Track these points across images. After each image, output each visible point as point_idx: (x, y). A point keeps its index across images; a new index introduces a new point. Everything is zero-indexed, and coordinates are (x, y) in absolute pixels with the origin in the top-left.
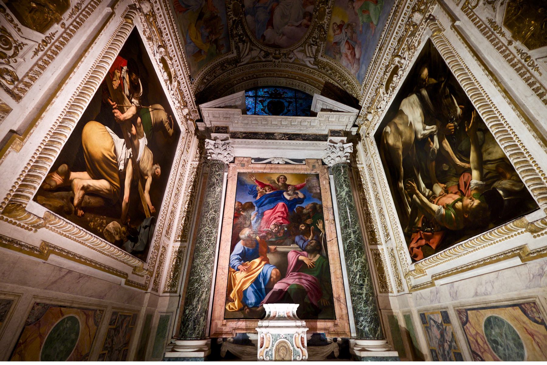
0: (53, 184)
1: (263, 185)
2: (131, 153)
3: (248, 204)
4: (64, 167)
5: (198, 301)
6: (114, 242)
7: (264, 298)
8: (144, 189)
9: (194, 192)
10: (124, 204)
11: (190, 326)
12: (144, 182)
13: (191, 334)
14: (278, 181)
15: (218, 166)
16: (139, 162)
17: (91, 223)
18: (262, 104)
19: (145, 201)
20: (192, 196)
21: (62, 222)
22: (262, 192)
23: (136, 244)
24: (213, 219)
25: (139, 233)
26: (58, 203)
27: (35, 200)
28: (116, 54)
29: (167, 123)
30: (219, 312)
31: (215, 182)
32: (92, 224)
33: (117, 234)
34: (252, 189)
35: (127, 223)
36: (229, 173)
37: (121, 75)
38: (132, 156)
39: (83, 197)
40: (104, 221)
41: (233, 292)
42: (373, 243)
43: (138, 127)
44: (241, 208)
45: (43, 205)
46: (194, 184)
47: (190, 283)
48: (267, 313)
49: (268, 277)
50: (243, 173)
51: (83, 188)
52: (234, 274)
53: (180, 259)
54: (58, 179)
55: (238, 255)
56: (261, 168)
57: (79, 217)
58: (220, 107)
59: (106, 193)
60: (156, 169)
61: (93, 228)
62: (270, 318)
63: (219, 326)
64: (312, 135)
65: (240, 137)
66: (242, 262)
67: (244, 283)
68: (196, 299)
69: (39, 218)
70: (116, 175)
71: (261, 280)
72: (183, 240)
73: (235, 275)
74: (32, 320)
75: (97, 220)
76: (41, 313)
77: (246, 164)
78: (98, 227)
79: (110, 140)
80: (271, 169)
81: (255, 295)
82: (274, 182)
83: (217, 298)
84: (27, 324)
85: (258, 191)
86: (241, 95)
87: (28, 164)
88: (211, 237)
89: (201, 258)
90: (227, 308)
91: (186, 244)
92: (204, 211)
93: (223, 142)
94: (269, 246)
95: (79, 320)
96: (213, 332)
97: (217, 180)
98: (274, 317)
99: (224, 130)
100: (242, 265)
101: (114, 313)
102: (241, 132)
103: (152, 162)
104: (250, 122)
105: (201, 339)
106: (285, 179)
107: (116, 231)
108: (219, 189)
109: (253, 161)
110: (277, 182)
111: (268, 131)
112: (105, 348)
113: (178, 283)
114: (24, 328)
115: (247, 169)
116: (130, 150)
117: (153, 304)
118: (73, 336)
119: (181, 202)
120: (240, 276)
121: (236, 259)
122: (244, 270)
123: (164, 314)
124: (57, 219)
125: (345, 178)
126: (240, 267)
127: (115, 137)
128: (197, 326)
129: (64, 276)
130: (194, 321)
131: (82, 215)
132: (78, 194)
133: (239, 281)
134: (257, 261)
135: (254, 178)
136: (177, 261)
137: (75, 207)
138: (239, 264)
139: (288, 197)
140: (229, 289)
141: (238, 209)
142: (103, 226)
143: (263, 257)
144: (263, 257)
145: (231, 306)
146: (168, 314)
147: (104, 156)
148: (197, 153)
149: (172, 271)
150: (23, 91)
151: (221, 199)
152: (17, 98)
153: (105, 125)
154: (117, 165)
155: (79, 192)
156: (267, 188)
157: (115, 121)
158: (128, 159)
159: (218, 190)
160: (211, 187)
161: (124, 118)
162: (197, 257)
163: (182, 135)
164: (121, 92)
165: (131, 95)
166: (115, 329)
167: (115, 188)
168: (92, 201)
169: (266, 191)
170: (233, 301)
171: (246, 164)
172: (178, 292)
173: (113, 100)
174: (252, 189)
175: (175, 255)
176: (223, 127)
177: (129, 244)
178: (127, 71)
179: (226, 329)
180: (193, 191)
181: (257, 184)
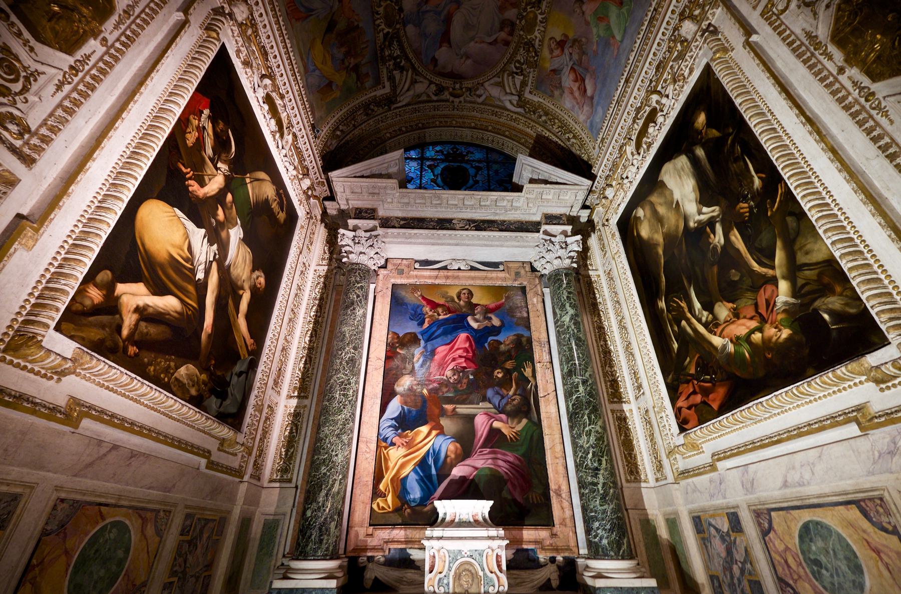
0: (88, 303)
1: (434, 305)
2: (217, 252)
3: (409, 336)
4: (105, 275)
5: (327, 495)
7: (435, 490)
8: (238, 312)
9: (319, 317)
10: (204, 336)
11: (313, 537)
12: (238, 299)
13: (315, 551)
14: (459, 297)
16: (229, 266)
17: (149, 367)
18: (432, 171)
19: (239, 330)
21: (102, 366)
22: (433, 316)
24: (352, 360)
25: (228, 384)
26: (96, 334)
27: (58, 328)
28: (192, 88)
29: (276, 202)
30: (362, 513)
32: (152, 368)
33: (193, 386)
37: (199, 124)
38: (217, 256)
39: (137, 325)
40: (172, 364)
42: (615, 400)
44: (397, 343)
45: (71, 337)
47: (313, 465)
48: (441, 516)
49: (443, 455)
51: (137, 310)
52: (385, 452)
53: (296, 426)
54: (95, 294)
55: (392, 419)
56: (430, 277)
57: (130, 357)
59: (174, 317)
60: (257, 278)
62: (445, 524)
63: (361, 537)
64: (515, 222)
65: (397, 225)
66: (400, 431)
67: (403, 466)
68: (323, 493)
69: (64, 359)
70: (191, 288)
71: (431, 461)
72: (302, 394)
73: (387, 453)
75: (161, 362)
76: (67, 516)
78: (162, 373)
79: (182, 231)
80: (447, 277)
82: (453, 300)
83: (357, 491)
85: (425, 315)
88: (348, 390)
90: (375, 507)
91: (306, 402)
94: (444, 406)
97: (358, 296)
98: (453, 521)
100: (400, 436)
101: (188, 516)
104: (412, 201)
105: (331, 559)
106: (471, 294)
107: (191, 380)
108: (361, 312)
109: (417, 266)
110: (456, 300)
111: (442, 216)
112: (173, 573)
115: (408, 278)
116: (215, 247)
117: (253, 500)
118: (120, 553)
119: (298, 333)
120: (395, 455)
121: (390, 426)
122: (403, 444)
125: (569, 293)
126: (396, 440)
131: (136, 355)
132: (129, 320)
134: (424, 429)
135: (419, 293)
136: (291, 429)
137: (124, 341)
138: (394, 435)
139: (475, 325)
140: (378, 476)
141: (393, 344)
142: (169, 373)
143: (434, 424)
144: (434, 424)
145: (381, 504)
146: (277, 517)
149: (283, 446)
150: (39, 150)
152: (29, 161)
153: (173, 205)
154: (193, 272)
155: (130, 315)
156: (440, 310)
157: (190, 198)
158: (211, 262)
159: (359, 312)
160: (347, 307)
161: (205, 194)
164: (200, 151)
167: (190, 310)
168: (152, 330)
169: (439, 315)
170: (384, 495)
171: (406, 270)
174: (416, 312)
176: (368, 209)
178: (209, 117)
179: (372, 542)
180: (319, 314)
181: (424, 303)
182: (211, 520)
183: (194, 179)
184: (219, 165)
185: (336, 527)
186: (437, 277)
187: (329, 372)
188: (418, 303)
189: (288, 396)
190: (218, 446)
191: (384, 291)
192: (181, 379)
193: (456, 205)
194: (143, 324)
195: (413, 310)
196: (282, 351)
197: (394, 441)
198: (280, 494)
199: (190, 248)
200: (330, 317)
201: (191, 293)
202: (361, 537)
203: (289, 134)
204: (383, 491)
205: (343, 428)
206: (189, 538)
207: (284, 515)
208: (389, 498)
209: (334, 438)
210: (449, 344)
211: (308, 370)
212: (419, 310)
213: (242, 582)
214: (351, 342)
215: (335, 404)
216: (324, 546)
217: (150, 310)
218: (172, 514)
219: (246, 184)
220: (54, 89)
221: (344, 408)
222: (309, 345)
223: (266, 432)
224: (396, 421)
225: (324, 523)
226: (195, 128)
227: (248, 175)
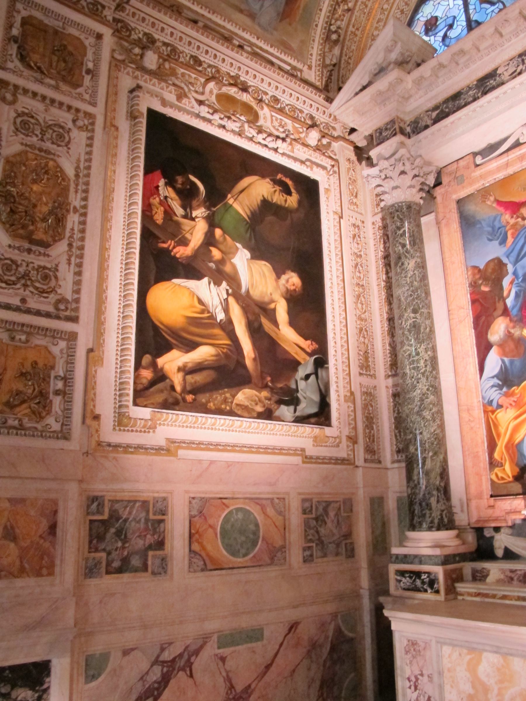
0: (145, 381)
2: (228, 288)
4: (147, 359)
6: (256, 416)
8: (276, 323)
10: (249, 363)
11: (416, 512)
12: (271, 315)
13: (420, 524)
15: (398, 216)
16: (248, 291)
17: (209, 404)
19: (286, 341)
21: (170, 415)
22: (516, 224)
23: (298, 408)
26: (160, 398)
27: (135, 404)
28: (141, 173)
29: (277, 193)
31: (401, 251)
32: (211, 404)
33: (257, 404)
34: (493, 227)
35: (267, 383)
37: (160, 199)
38: (230, 291)
39: (184, 380)
40: (228, 395)
41: (498, 449)
43: (222, 243)
44: (480, 278)
45: (145, 406)
50: (469, 196)
51: (179, 369)
52: (493, 417)
54: (147, 374)
55: (493, 377)
56: (499, 169)
57: (190, 403)
58: (364, 88)
59: (213, 360)
60: (287, 281)
61: (216, 409)
66: (505, 389)
67: (516, 429)
69: (146, 420)
70: (217, 331)
73: (496, 417)
74: (195, 512)
75: (217, 398)
76: (201, 506)
78: (222, 404)
79: (187, 293)
85: (505, 227)
87: (116, 372)
88: (418, 361)
89: (409, 404)
93: (392, 161)
95: (252, 511)
99: (390, 129)
100: (506, 395)
103: (274, 276)
107: (252, 401)
109: (479, 160)
111: (481, 74)
114: (190, 521)
116: (224, 284)
121: (493, 386)
122: (511, 405)
124: (165, 415)
126: (503, 401)
127: (192, 284)
128: (428, 512)
129: (207, 468)
130: (420, 504)
131: (194, 400)
132: (177, 380)
133: (504, 428)
135: (492, 198)
137: (181, 395)
138: (499, 396)
140: (492, 446)
141: (475, 283)
142: (228, 402)
145: (500, 475)
147: (188, 318)
150: (77, 309)
152: (75, 319)
153: (169, 279)
154: (212, 317)
155: (176, 376)
157: (181, 264)
158: (226, 300)
161: (193, 249)
164: (171, 220)
165: (188, 210)
166: (317, 519)
167: (223, 348)
168: (199, 378)
173: (165, 240)
174: (493, 227)
176: (387, 124)
177: (286, 411)
178: (166, 184)
179: (497, 513)
181: (502, 209)
182: (333, 501)
183: (177, 246)
184: (194, 214)
186: (507, 165)
189: (385, 376)
190: (312, 443)
192: (242, 403)
193: (492, 45)
194: (189, 377)
195: (489, 226)
197: (500, 403)
199: (200, 302)
201: (218, 335)
203: (262, 108)
204: (499, 460)
205: (421, 405)
206: (313, 516)
208: (507, 467)
209: (415, 417)
217: (190, 365)
218: (287, 501)
219: (231, 206)
220: (67, 266)
221: (418, 382)
223: (372, 418)
224: (500, 380)
225: (424, 498)
226: (158, 205)
227: (229, 196)
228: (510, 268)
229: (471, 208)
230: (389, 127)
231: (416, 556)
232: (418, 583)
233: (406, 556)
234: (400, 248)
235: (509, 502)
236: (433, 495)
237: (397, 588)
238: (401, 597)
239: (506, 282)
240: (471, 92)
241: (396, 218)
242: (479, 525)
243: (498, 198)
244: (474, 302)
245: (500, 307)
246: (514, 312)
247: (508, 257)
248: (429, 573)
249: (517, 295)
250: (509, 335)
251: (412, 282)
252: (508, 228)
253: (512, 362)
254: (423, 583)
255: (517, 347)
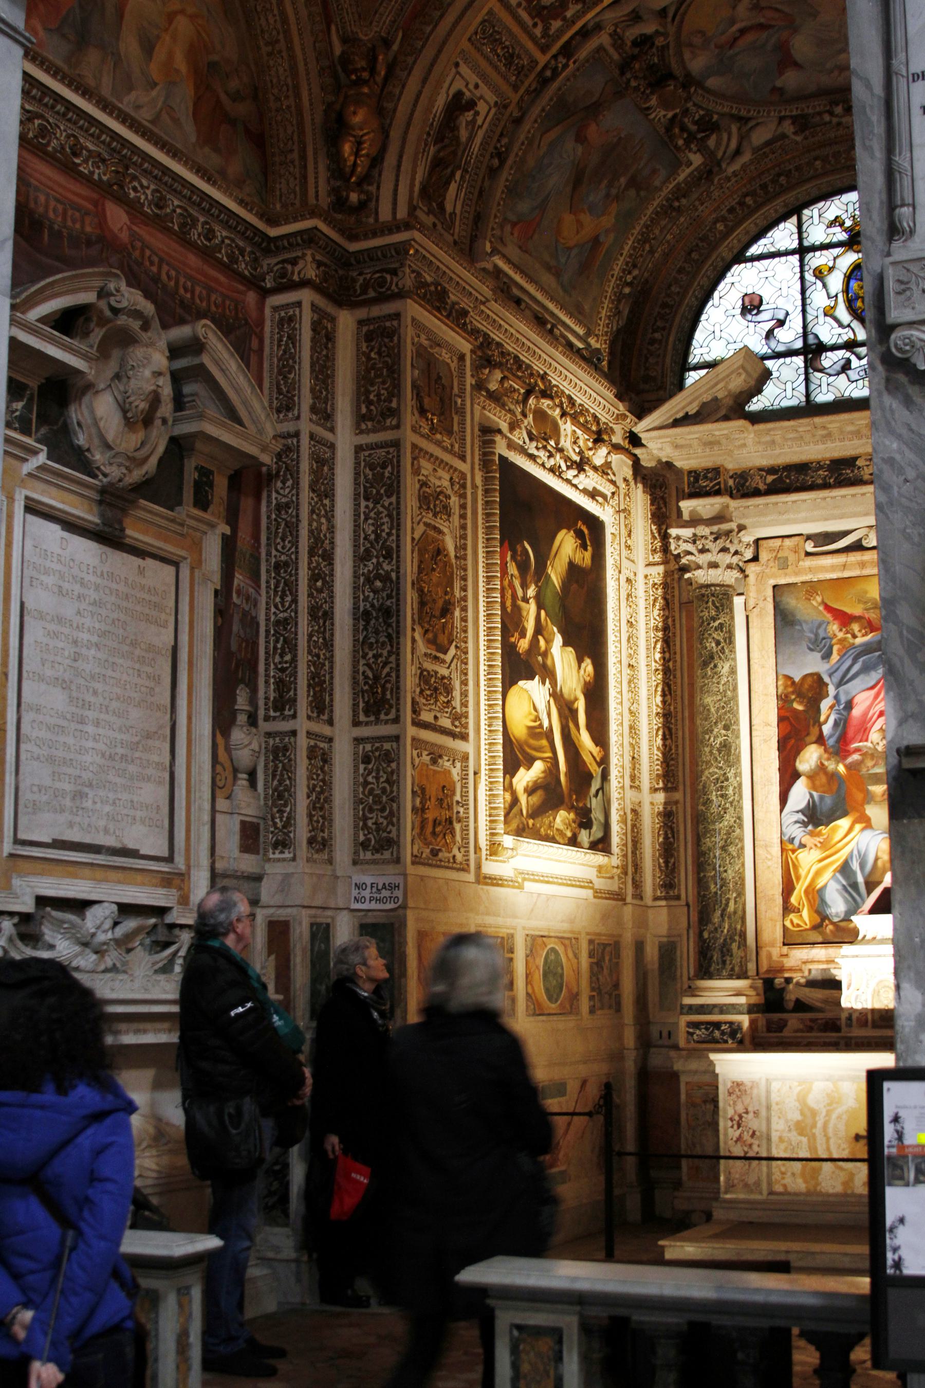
1: (845, 619)
3: (809, 680)
5: (722, 915)
7: (863, 902)
9: (669, 661)
10: (563, 778)
15: (713, 602)
20: (667, 671)
22: (845, 639)
24: (725, 746)
25: (590, 811)
30: (773, 932)
31: (715, 650)
36: (748, 596)
41: (796, 893)
44: (793, 693)
46: (664, 635)
47: (701, 884)
50: (788, 585)
52: (793, 856)
53: (672, 829)
56: (833, 568)
63: (775, 958)
65: (762, 487)
66: (810, 827)
67: (818, 873)
68: (718, 913)
71: (855, 866)
72: (670, 785)
77: (792, 558)
81: (844, 898)
83: (762, 907)
84: (527, 956)
85: (831, 639)
86: (740, 363)
88: (726, 788)
90: (788, 924)
91: (678, 796)
92: (700, 730)
94: (870, 788)
96: (764, 966)
97: (718, 643)
98: (874, 938)
100: (811, 834)
101: (591, 942)
102: (760, 469)
104: (778, 439)
105: (738, 978)
109: (809, 547)
111: (837, 454)
112: (593, 989)
113: (679, 881)
115: (796, 574)
117: (641, 923)
118: (559, 969)
119: (643, 692)
120: (807, 860)
121: (796, 822)
123: (665, 939)
126: (806, 840)
128: (728, 958)
134: (844, 823)
135: (819, 599)
136: (666, 834)
140: (788, 888)
141: (786, 696)
143: (857, 815)
144: (857, 815)
145: (796, 921)
146: (672, 939)
148: (654, 537)
149: (660, 855)
151: (735, 689)
156: (855, 627)
159: (725, 668)
160: (705, 664)
162: (705, 834)
163: (609, 530)
169: (854, 636)
170: (798, 911)
171: (792, 558)
172: (683, 896)
174: (816, 635)
175: (657, 722)
177: (584, 837)
180: (667, 655)
181: (829, 617)
185: (739, 948)
186: (844, 567)
187: (697, 765)
188: (820, 619)
191: (761, 604)
195: (811, 632)
196: (628, 641)
198: (669, 914)
200: (685, 658)
202: (775, 957)
207: (680, 936)
208: (805, 913)
210: (872, 688)
211: (671, 749)
212: (822, 634)
213: (650, 1006)
214: (720, 719)
215: (714, 809)
216: (729, 967)
222: (664, 709)
224: (804, 814)
228: (832, 690)
229: (792, 602)
230: (709, 475)
231: (715, 1006)
232: (717, 1034)
233: (702, 1006)
234: (713, 645)
235: (806, 951)
236: (735, 941)
237: (688, 1042)
238: (695, 1050)
239: (825, 705)
240: (821, 472)
241: (710, 604)
242: (770, 976)
243: (826, 601)
244: (781, 719)
245: (814, 732)
246: (831, 742)
247: (830, 676)
248: (731, 1023)
249: (836, 724)
250: (821, 767)
251: (725, 691)
252: (834, 641)
253: (821, 798)
254: (723, 1033)
255: (829, 783)
